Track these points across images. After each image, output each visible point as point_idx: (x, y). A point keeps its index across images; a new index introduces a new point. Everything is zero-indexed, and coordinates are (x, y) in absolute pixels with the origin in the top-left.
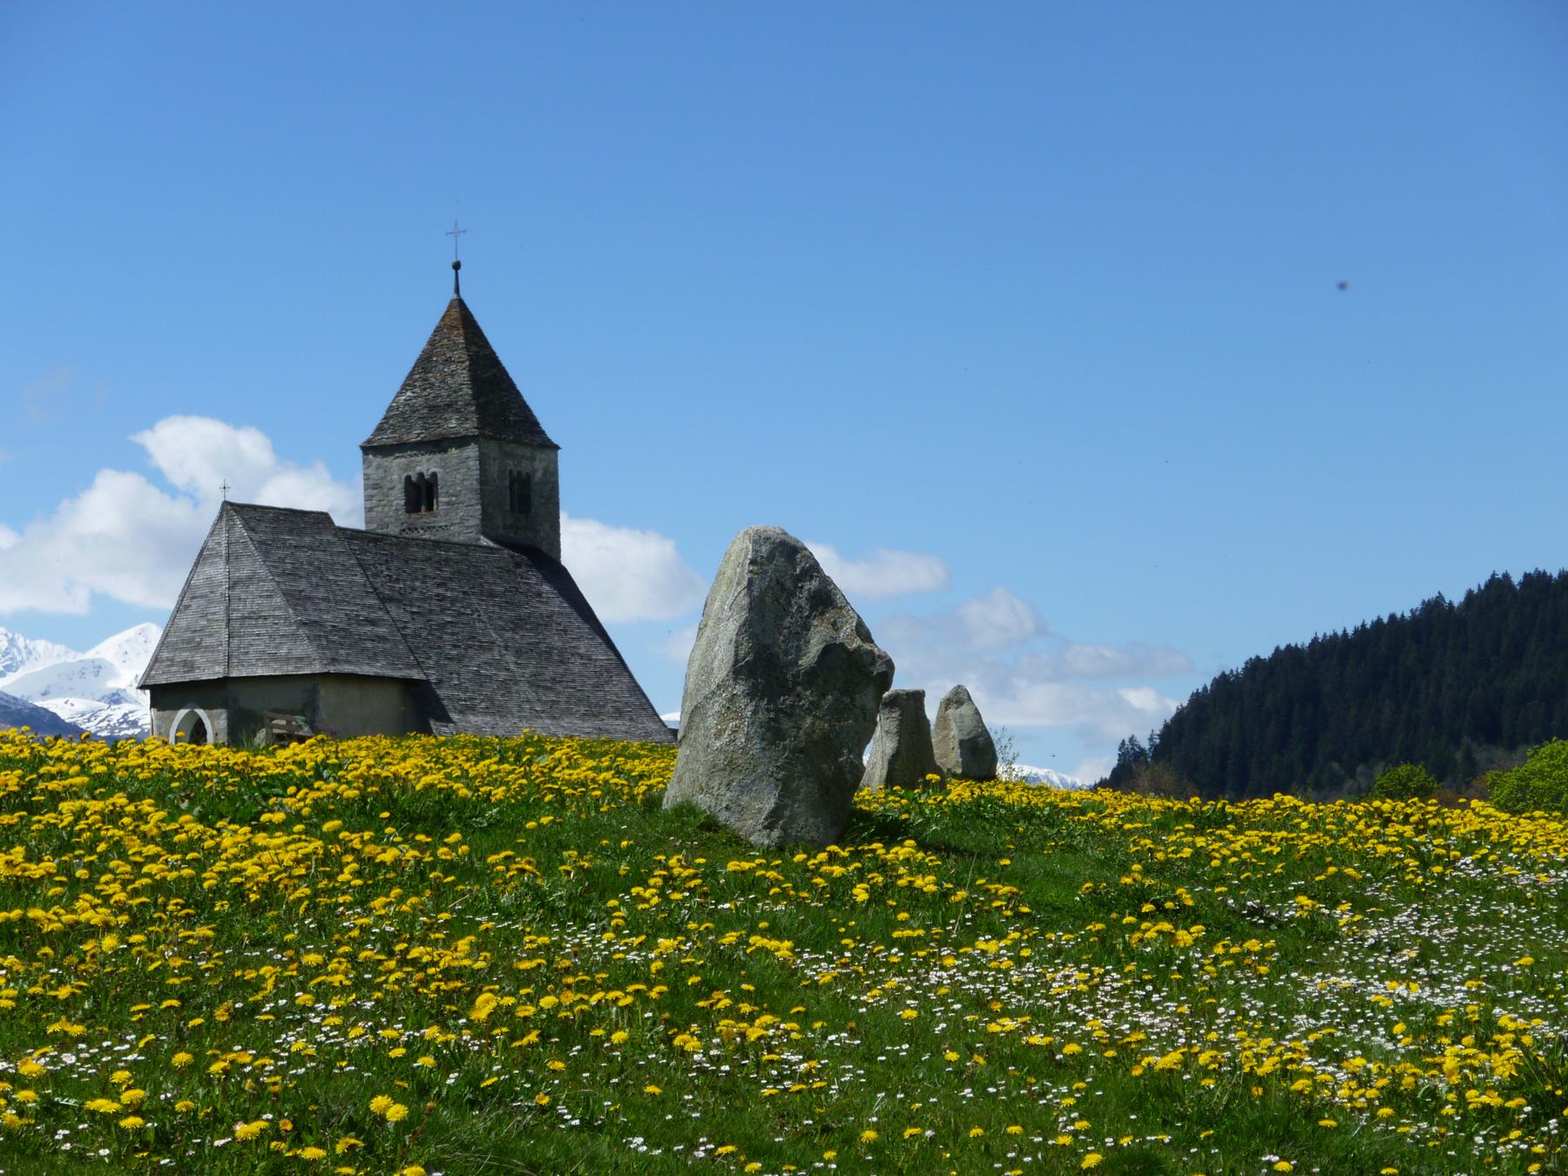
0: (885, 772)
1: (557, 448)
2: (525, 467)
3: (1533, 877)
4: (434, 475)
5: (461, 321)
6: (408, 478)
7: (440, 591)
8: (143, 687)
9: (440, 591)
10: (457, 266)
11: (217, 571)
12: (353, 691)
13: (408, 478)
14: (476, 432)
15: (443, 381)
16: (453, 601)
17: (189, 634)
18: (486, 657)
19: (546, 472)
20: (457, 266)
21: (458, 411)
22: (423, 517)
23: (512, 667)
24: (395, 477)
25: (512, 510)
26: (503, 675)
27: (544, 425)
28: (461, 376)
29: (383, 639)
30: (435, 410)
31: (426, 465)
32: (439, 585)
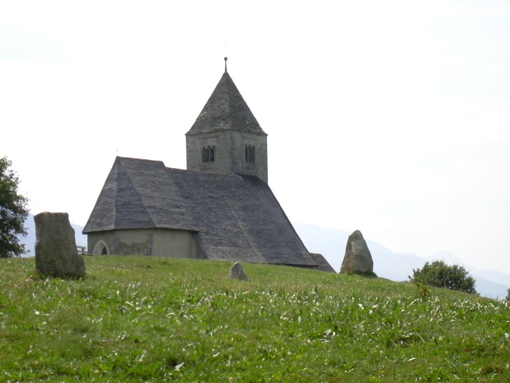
0: (106, 230)
1: (267, 135)
2: (252, 143)
3: (424, 286)
4: (214, 146)
5: (226, 89)
6: (204, 148)
7: (210, 194)
8: (84, 233)
9: (210, 194)
10: (226, 59)
11: (114, 185)
12: (168, 236)
13: (204, 148)
14: (230, 128)
15: (219, 107)
16: (216, 199)
17: (101, 212)
18: (229, 222)
19: (262, 145)
20: (226, 59)
21: (224, 119)
22: (209, 165)
23: (241, 226)
24: (198, 147)
25: (247, 161)
26: (236, 230)
27: (261, 126)
28: (226, 107)
29: (182, 214)
30: (215, 119)
31: (211, 142)
32: (210, 192)
